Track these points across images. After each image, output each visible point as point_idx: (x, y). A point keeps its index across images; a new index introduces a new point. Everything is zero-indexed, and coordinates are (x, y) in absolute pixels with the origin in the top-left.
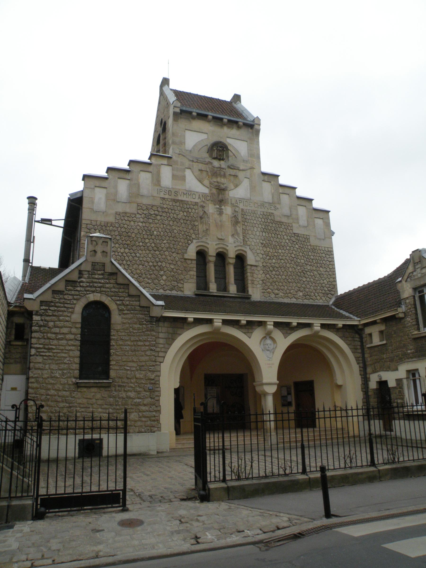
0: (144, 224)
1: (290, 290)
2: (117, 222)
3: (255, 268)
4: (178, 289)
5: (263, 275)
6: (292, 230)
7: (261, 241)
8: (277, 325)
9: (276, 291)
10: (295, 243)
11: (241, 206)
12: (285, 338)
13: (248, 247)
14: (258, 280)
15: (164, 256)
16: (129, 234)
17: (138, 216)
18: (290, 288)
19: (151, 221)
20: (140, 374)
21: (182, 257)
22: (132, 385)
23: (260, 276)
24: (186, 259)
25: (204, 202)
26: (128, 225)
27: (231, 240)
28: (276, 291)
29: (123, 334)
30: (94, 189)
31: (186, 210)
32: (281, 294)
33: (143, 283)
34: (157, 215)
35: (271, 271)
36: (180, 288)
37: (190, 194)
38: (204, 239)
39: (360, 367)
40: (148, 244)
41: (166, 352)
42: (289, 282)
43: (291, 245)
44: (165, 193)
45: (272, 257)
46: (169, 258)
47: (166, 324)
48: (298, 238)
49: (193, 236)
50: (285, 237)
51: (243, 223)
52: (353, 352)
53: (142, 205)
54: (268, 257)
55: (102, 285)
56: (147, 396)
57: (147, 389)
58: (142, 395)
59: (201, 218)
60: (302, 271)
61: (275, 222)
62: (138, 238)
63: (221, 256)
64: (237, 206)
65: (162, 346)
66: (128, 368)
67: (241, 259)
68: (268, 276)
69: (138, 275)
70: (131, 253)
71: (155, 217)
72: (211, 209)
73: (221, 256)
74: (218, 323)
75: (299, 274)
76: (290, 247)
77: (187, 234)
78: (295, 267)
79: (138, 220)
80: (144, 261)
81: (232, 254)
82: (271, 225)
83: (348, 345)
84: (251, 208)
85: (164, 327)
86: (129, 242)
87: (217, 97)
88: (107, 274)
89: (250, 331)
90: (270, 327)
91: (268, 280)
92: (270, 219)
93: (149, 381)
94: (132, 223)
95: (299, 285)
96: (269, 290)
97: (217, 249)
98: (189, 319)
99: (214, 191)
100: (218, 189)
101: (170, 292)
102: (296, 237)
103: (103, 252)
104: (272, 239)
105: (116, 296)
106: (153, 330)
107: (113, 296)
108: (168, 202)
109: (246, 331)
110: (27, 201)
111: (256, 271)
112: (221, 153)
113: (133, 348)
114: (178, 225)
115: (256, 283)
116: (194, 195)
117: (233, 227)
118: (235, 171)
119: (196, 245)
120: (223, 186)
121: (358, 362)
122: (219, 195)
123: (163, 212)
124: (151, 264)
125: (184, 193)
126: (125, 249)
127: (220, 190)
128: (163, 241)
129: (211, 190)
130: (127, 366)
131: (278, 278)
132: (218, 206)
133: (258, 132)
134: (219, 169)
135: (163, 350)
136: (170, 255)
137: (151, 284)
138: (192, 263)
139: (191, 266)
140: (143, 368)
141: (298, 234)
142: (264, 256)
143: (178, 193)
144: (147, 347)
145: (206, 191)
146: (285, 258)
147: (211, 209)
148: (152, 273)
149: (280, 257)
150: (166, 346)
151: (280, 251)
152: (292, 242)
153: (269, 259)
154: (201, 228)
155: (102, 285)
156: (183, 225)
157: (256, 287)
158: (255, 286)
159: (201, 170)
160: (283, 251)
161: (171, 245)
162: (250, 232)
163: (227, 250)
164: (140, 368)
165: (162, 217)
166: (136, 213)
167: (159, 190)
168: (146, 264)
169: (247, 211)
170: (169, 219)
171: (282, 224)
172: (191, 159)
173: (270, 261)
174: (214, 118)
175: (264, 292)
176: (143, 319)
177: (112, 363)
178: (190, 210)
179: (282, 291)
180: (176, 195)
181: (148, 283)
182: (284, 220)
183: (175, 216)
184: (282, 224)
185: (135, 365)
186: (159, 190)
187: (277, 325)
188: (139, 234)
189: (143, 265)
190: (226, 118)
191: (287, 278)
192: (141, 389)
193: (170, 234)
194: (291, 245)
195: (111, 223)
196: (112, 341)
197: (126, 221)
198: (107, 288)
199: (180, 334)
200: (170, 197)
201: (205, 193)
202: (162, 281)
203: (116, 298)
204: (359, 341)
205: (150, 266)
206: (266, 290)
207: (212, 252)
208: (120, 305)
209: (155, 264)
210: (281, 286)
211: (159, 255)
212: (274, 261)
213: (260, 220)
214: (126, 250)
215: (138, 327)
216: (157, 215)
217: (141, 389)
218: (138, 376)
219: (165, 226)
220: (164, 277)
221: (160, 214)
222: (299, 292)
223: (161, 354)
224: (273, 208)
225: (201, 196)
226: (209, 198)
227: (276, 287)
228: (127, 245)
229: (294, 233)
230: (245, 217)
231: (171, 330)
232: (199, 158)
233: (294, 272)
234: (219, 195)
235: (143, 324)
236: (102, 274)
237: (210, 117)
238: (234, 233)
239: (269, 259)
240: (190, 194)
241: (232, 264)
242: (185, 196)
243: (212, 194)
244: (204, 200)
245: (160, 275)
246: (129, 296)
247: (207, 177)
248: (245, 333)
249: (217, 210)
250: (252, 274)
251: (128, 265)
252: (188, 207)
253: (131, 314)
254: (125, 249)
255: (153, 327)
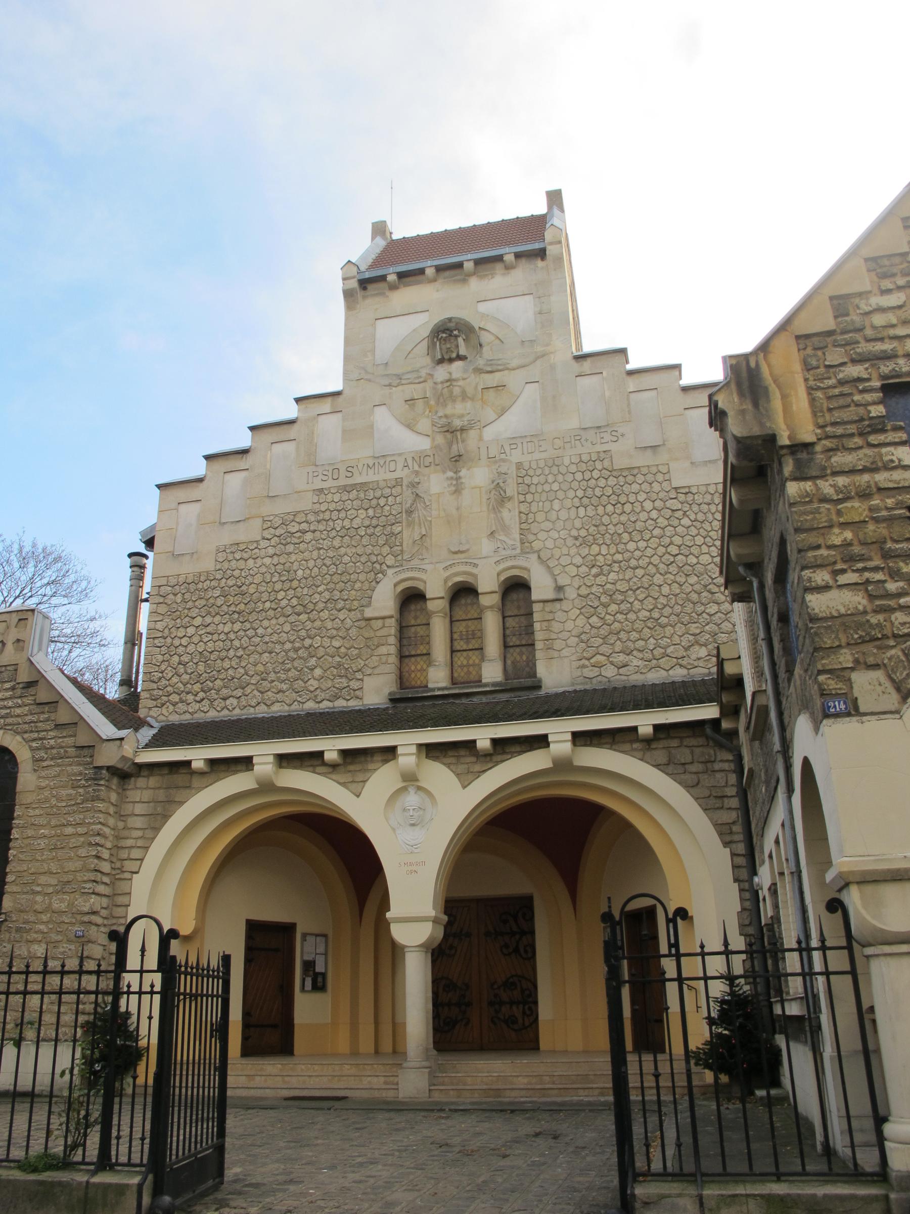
0: (276, 560)
1: (665, 648)
2: (218, 568)
3: (557, 605)
4: (349, 694)
5: (581, 621)
6: (669, 480)
7: (574, 533)
8: (431, 750)
9: (622, 658)
10: (679, 514)
11: (516, 456)
12: (464, 787)
13: (534, 557)
14: (565, 635)
15: (318, 624)
16: (244, 588)
17: (264, 544)
18: (663, 642)
19: (290, 548)
20: (62, 901)
21: (360, 616)
22: (42, 927)
23: (570, 625)
24: (369, 619)
25: (417, 473)
26: (241, 570)
27: (487, 547)
28: (622, 658)
29: (37, 812)
30: (177, 509)
31: (374, 502)
32: (636, 662)
33: (269, 693)
34: (304, 532)
35: (606, 606)
36: (355, 690)
37: (382, 463)
38: (415, 562)
39: (733, 855)
40: (284, 603)
41: (147, 848)
42: (663, 627)
43: (666, 523)
44: (325, 478)
45: (606, 568)
46: (329, 624)
47: (153, 781)
48: (690, 498)
49: (390, 560)
50: (648, 505)
51: (522, 498)
52: (705, 810)
53: (272, 518)
54: (594, 571)
55: (8, 711)
56: (69, 953)
57: (72, 936)
58: (61, 950)
59: (409, 512)
60: (705, 586)
61: (615, 473)
62: (261, 593)
63: (463, 592)
64: (504, 460)
65: (139, 833)
66: (39, 889)
67: (516, 588)
68: (594, 620)
69: (258, 678)
70: (245, 631)
71: (299, 538)
72: (436, 483)
73: (463, 592)
74: (264, 766)
75: (694, 596)
76: (663, 529)
77: (374, 559)
78: (678, 579)
79: (263, 552)
80: (273, 642)
81: (488, 583)
82: (602, 482)
83: (688, 787)
84: (543, 455)
85: (147, 788)
86: (242, 607)
87: (514, 216)
88: (21, 686)
89: (360, 777)
90: (407, 759)
91: (594, 631)
92: (600, 467)
93: (78, 917)
94: (251, 563)
95: (693, 628)
96: (599, 658)
97: (446, 581)
98: (195, 765)
99: (440, 439)
100: (448, 431)
101: (330, 704)
102: (682, 497)
103: (18, 640)
104: (606, 520)
105: (32, 732)
106: (98, 799)
107: (26, 732)
108: (330, 497)
109: (343, 778)
110: (128, 561)
111: (559, 614)
112: (448, 346)
113: (53, 841)
114: (353, 543)
115: (558, 645)
116: (393, 464)
117: (492, 516)
118: (497, 375)
119: (395, 581)
120: (457, 423)
121: (728, 838)
122: (453, 446)
123: (319, 522)
124: (288, 646)
125: (368, 466)
126: (233, 623)
127: (452, 432)
128: (318, 587)
129: (433, 440)
130: (38, 885)
131: (626, 619)
132: (450, 474)
133: (561, 263)
134: (448, 384)
135: (140, 843)
136: (332, 617)
137: (287, 693)
138: (384, 626)
139: (384, 632)
140: (68, 888)
141: (689, 487)
142: (584, 569)
143: (354, 470)
144: (82, 839)
145: (424, 444)
146: (647, 560)
147: (436, 483)
148: (289, 666)
149: (633, 563)
150: (149, 833)
151: (631, 546)
152: (668, 513)
153: (596, 576)
154: (408, 536)
155: (8, 711)
156: (365, 541)
157: (560, 657)
158: (556, 654)
159: (410, 401)
160: (642, 544)
161: (336, 592)
162: (540, 517)
163: (475, 576)
164: (63, 887)
165: (317, 534)
166: (259, 538)
167: (311, 474)
168: (278, 648)
169: (534, 466)
170: (334, 533)
171: (635, 471)
172: (387, 383)
173: (601, 580)
174: (439, 269)
175: (584, 666)
176: (81, 774)
177: (10, 878)
178: (382, 502)
179: (641, 656)
180: (349, 474)
181: (280, 691)
182: (643, 460)
183: (347, 523)
184: (635, 471)
185: (54, 881)
186: (311, 474)
187: (431, 750)
188: (263, 584)
189: (270, 653)
190: (468, 258)
191: (656, 614)
192: (59, 938)
193: (333, 569)
194: (666, 523)
195: (207, 572)
196: (14, 831)
197: (238, 560)
198: (18, 716)
199: (181, 803)
200: (336, 483)
201: (422, 452)
202: (312, 682)
203: (31, 734)
204: (734, 772)
205: (286, 652)
206: (589, 659)
207: (435, 589)
208: (38, 749)
209: (297, 645)
210: (634, 642)
211: (308, 622)
212: (612, 576)
213: (570, 478)
214: (235, 625)
215: (67, 795)
216: (304, 532)
217: (59, 938)
218: (56, 905)
219: (321, 552)
220: (318, 672)
221: (312, 528)
222: (697, 647)
223: (136, 853)
224: (607, 437)
225: (410, 462)
226: (431, 459)
227: (618, 646)
228: (239, 613)
229: (676, 488)
230: (527, 480)
231: (161, 795)
232: (403, 374)
233: (676, 595)
234: (450, 444)
235: (79, 787)
236: (13, 688)
237: (430, 272)
238: (494, 528)
239: (596, 576)
240: (382, 463)
241: (491, 607)
242: (371, 472)
243: (436, 447)
244: (416, 468)
245: (307, 667)
246: (58, 726)
247: (427, 412)
248: (343, 784)
249: (449, 482)
250: (545, 624)
251: (238, 657)
252: (378, 494)
253: (59, 766)
254: (233, 623)
255: (99, 790)
